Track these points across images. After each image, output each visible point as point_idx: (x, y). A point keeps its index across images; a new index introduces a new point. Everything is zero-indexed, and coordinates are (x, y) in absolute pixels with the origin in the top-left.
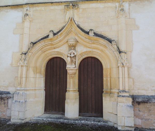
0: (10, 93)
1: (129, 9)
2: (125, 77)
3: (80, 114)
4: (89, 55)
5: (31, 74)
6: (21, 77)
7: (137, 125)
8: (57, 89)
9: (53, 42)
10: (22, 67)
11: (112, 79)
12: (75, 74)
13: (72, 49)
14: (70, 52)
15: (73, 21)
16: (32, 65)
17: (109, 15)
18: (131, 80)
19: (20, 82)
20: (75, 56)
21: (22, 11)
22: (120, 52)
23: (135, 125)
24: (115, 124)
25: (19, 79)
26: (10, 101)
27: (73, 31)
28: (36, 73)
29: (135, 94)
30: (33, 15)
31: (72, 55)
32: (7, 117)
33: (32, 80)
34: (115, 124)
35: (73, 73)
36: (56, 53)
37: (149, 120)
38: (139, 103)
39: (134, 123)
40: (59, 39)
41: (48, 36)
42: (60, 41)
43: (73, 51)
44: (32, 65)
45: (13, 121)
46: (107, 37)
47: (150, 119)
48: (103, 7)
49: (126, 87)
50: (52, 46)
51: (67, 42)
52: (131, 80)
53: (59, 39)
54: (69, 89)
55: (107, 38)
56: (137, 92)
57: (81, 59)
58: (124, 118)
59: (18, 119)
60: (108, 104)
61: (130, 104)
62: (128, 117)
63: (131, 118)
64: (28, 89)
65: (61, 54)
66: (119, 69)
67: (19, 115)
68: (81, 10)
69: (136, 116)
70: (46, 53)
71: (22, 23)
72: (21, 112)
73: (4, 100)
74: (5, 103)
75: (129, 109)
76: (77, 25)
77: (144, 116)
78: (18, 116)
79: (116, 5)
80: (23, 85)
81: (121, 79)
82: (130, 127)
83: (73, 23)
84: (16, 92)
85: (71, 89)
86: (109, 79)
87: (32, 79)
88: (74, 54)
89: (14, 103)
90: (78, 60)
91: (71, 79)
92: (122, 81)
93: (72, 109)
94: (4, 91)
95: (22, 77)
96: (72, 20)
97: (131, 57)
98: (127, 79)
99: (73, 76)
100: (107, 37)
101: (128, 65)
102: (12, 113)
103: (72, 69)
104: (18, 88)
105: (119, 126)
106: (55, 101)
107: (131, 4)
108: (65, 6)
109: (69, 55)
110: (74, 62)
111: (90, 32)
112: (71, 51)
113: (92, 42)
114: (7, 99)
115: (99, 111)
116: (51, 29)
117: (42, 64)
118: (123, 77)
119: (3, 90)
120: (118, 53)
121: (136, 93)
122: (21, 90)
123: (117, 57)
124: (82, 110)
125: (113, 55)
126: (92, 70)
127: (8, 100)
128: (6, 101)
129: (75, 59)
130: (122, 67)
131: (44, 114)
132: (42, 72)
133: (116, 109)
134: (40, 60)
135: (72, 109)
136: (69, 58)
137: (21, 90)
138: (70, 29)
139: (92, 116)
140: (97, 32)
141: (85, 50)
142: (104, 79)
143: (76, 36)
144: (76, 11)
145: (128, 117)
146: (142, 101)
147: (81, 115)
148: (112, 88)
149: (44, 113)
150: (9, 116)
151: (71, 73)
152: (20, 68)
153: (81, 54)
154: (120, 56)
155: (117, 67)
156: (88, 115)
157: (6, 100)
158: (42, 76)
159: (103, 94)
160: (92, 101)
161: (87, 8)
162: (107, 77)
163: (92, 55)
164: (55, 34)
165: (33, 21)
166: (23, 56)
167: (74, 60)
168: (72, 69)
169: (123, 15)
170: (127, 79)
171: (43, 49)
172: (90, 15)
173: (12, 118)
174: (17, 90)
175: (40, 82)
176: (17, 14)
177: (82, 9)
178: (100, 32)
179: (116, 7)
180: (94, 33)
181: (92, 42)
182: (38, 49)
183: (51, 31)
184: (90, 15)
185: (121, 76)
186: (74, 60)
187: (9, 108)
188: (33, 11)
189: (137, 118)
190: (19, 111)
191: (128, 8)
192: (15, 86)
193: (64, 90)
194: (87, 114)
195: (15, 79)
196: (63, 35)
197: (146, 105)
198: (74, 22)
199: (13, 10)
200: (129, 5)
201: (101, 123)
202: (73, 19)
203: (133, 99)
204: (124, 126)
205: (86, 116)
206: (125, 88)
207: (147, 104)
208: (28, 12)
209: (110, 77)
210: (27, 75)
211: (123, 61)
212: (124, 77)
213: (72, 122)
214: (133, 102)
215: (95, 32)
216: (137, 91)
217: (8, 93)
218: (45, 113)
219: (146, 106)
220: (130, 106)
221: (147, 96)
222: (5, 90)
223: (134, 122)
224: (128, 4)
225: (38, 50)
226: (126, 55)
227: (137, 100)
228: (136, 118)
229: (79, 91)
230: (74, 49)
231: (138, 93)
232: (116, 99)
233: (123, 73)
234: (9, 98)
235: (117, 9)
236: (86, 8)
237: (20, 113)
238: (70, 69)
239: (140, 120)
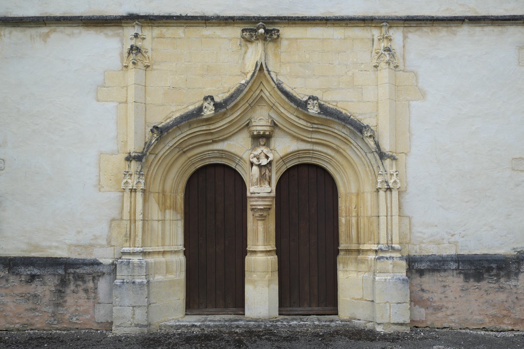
0: (101, 263)
1: (404, 46)
2: (393, 214)
3: (282, 309)
4: (303, 159)
5: (155, 212)
6: (133, 221)
7: (417, 321)
8: (217, 249)
9: (212, 127)
10: (133, 194)
11: (362, 220)
12: (270, 209)
13: (262, 143)
15: (266, 72)
16: (156, 187)
17: (355, 60)
18: (406, 221)
19: (129, 233)
20: (270, 163)
21: (118, 35)
22: (382, 156)
23: (412, 321)
24: (370, 322)
25: (126, 224)
26: (103, 284)
27: (265, 98)
28: (165, 210)
29: (413, 253)
30: (152, 50)
31: (264, 162)
32: (96, 325)
33: (157, 226)
34: (370, 322)
35: (265, 207)
36: (218, 155)
37: (441, 308)
38: (421, 273)
39: (410, 317)
41: (200, 110)
43: (265, 150)
44: (156, 187)
45: (117, 331)
46: (352, 117)
47: (443, 306)
48: (341, 38)
49: (393, 238)
50: (210, 137)
51: (248, 125)
52: (406, 221)
54: (255, 247)
55: (352, 119)
56: (417, 247)
58: (390, 307)
59: (131, 324)
60: (351, 280)
61: (403, 274)
62: (397, 303)
63: (404, 304)
64: (148, 249)
65: (231, 156)
66: (378, 196)
67: (134, 315)
69: (415, 301)
70: (190, 154)
71: (122, 70)
72: (139, 307)
73: (84, 282)
74: (86, 291)
75: (400, 286)
76: (276, 84)
77: (431, 300)
78: (133, 318)
79: (373, 36)
80: (137, 239)
81: (383, 219)
82: (402, 324)
83: (265, 76)
84: (120, 258)
85: (261, 248)
86: (354, 220)
88: (267, 157)
89: (120, 287)
90: (276, 173)
91: (260, 223)
93: (261, 297)
94: (81, 259)
95: (132, 218)
96: (261, 69)
97: (405, 166)
98: (396, 219)
99: (265, 214)
100: (352, 117)
101: (399, 185)
102: (114, 311)
103: (260, 191)
104: (126, 249)
105: (379, 324)
106: (213, 275)
107: (410, 35)
108: (243, 31)
109: (255, 160)
110: (268, 178)
111: (311, 102)
112: (258, 151)
113: (314, 129)
114: (94, 278)
115: (327, 297)
117: (174, 182)
118: (387, 214)
119: (78, 257)
120: (378, 157)
121: (415, 251)
122: (134, 254)
123: (375, 168)
124: (287, 299)
125: (365, 163)
126: (309, 199)
127: (96, 281)
128: (91, 284)
129: (270, 171)
130: (385, 191)
131: (186, 315)
132: (179, 206)
133: (368, 292)
135: (261, 297)
136: (255, 169)
137: (134, 254)
138: (258, 92)
139: (311, 313)
140: (326, 102)
141: (293, 146)
142: (342, 220)
143: (272, 111)
144: (271, 45)
145: (397, 303)
146: (429, 268)
147: (284, 313)
148: (362, 241)
149: (184, 313)
150: (102, 323)
151: (259, 207)
152: (127, 194)
153: (284, 159)
154: (383, 164)
155: (375, 192)
156: (301, 311)
157: (91, 282)
158: (179, 217)
159: (341, 257)
160: (310, 275)
161: (300, 39)
162: (348, 214)
163: (310, 159)
164: (217, 106)
165: (154, 67)
166: (134, 166)
167: (267, 173)
168: (260, 191)
169: (389, 65)
172: (307, 56)
173: (116, 323)
174: (124, 253)
175: (171, 232)
176: (109, 46)
177: (287, 39)
178: (334, 104)
179: (373, 40)
180: (321, 106)
181: (314, 129)
182: (171, 145)
183: (209, 99)
184: (307, 56)
185: (383, 212)
186: (267, 173)
187: (100, 301)
188: (153, 38)
189: (417, 306)
190: (133, 307)
191: (402, 44)
192: (113, 243)
193: (240, 250)
194: (297, 309)
195: (111, 224)
196: (239, 107)
197: (437, 276)
198: (268, 76)
199: (89, 32)
201: (337, 322)
202: (266, 67)
203: (409, 265)
204: (389, 324)
205: (297, 313)
206: (392, 239)
207: (438, 274)
208: (139, 43)
209: (358, 215)
210: (144, 214)
211: (388, 177)
212: (389, 214)
213: (268, 326)
214: (410, 270)
215: (322, 103)
216: (418, 246)
217: (95, 263)
218: (188, 313)
219: (436, 278)
220: (403, 280)
221: (440, 256)
222: (83, 257)
223: (411, 314)
224: (402, 35)
225: (171, 147)
226: (394, 162)
227: (417, 266)
228: (415, 305)
229: (279, 252)
230: (267, 145)
231: (420, 249)
232: (371, 267)
233: (389, 205)
234: (99, 276)
235: (375, 46)
236: (297, 39)
237: (138, 311)
238: (259, 197)
239: (423, 310)
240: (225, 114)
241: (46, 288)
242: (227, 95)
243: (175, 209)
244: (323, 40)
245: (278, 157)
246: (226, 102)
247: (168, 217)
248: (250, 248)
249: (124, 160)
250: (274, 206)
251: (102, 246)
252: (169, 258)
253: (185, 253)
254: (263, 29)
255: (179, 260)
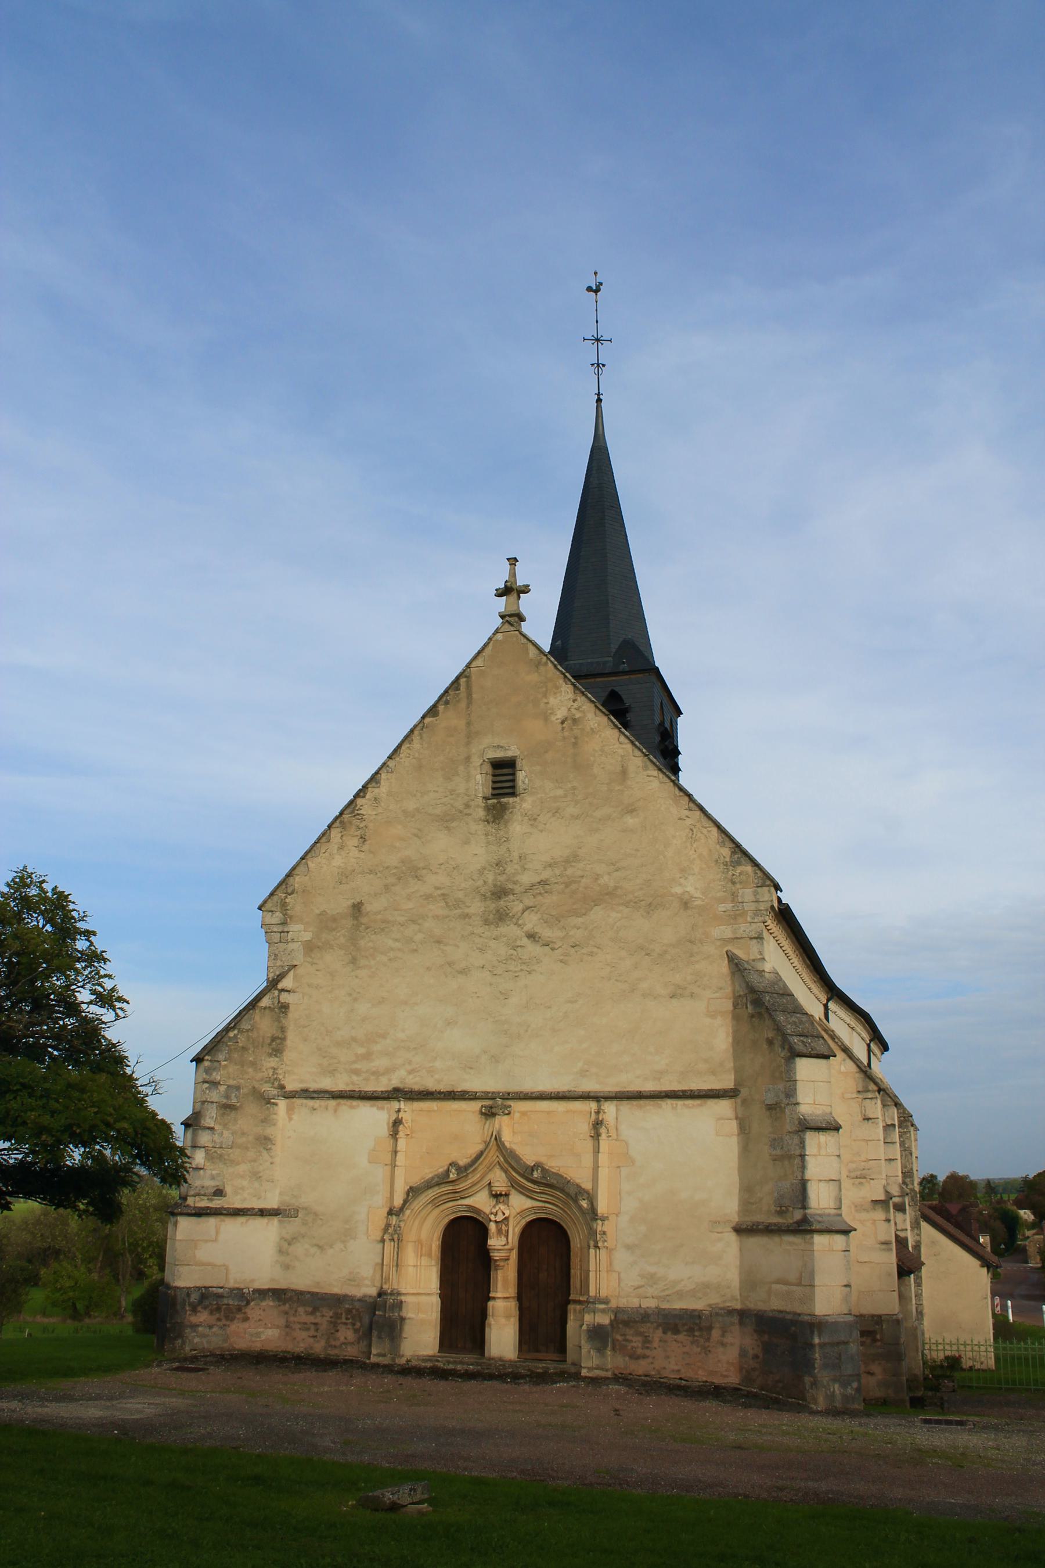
14: (494, 1211)
18: (615, 1275)
20: (507, 1219)
40: (470, 1181)
42: (474, 1185)
53: (470, 1181)
57: (523, 1223)
68: (517, 1115)
87: (411, 1270)
92: (431, 1085)
93: (503, 1337)
103: (503, 1244)
106: (462, 1321)
107: (621, 1108)
116: (453, 1159)
126: (552, 1250)
129: (507, 1225)
134: (426, 1229)
135: (503, 1337)
158: (433, 1263)
170: (604, 1274)
171: (640, 1290)
176: (374, 1118)
200: (617, 1110)
229: (520, 1298)
240: (466, 1176)
241: (323, 1318)
242: (469, 1160)
243: (430, 1255)
244: (549, 1113)
245: (514, 1212)
246: (466, 1168)
247: (423, 1263)
248: (492, 1295)
249: (935, 1174)
250: (514, 1255)
251: (367, 1286)
252: (423, 1299)
253: (440, 1296)
254: (494, 1105)
255: (435, 1301)
